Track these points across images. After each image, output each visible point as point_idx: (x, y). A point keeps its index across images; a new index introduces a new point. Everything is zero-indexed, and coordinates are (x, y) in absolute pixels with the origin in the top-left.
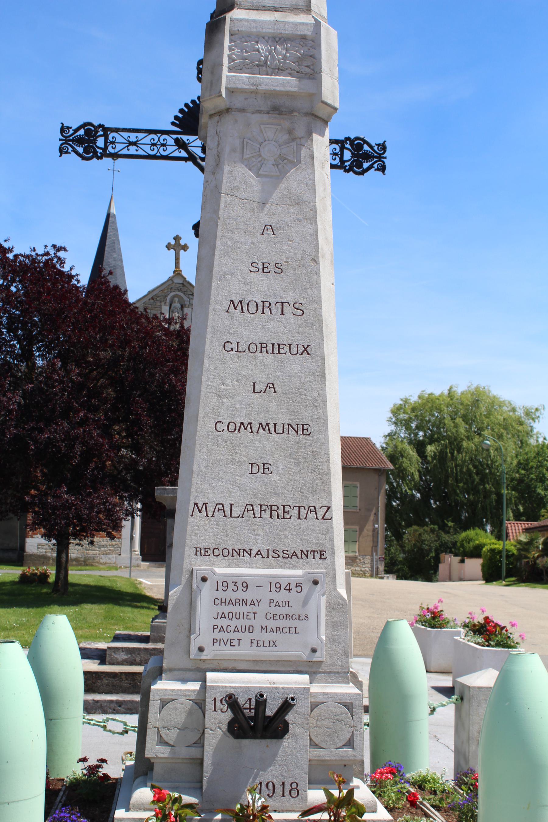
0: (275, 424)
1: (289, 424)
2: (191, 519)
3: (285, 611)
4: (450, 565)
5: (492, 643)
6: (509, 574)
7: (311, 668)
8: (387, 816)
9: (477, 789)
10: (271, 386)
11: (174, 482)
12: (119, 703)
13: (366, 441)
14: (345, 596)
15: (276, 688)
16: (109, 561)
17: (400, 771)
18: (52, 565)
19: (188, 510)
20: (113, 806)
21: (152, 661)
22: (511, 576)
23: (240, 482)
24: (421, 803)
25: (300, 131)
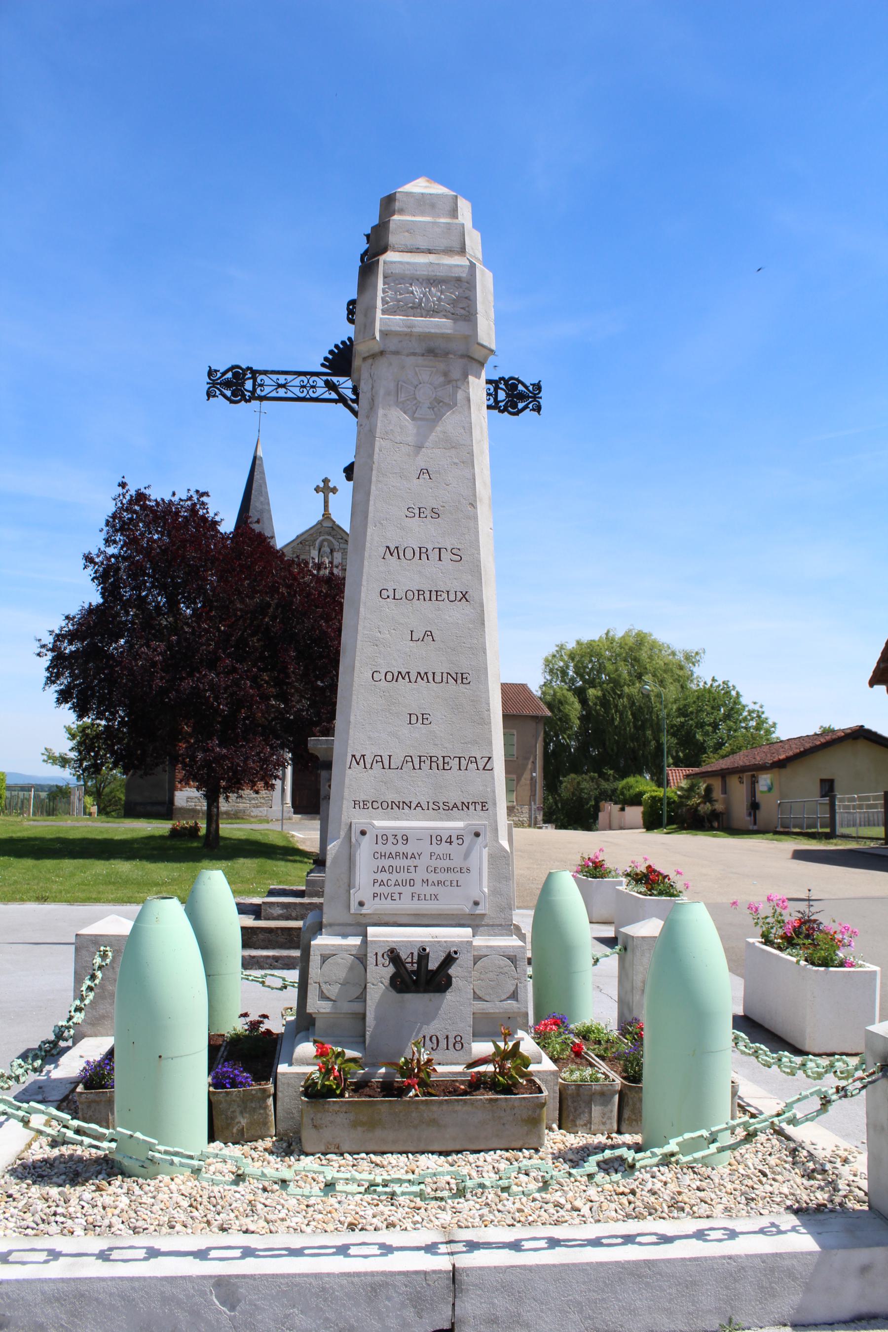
0: (434, 673)
2: (349, 772)
3: (446, 863)
4: (610, 813)
5: (655, 892)
6: (671, 821)
7: (473, 921)
8: (552, 1067)
9: (642, 1038)
11: (329, 731)
12: (276, 959)
13: (523, 688)
15: (439, 942)
16: (259, 814)
17: (564, 1022)
18: (202, 819)
20: (276, 1061)
21: (311, 917)
22: (673, 824)
24: (586, 1053)
25: (456, 374)
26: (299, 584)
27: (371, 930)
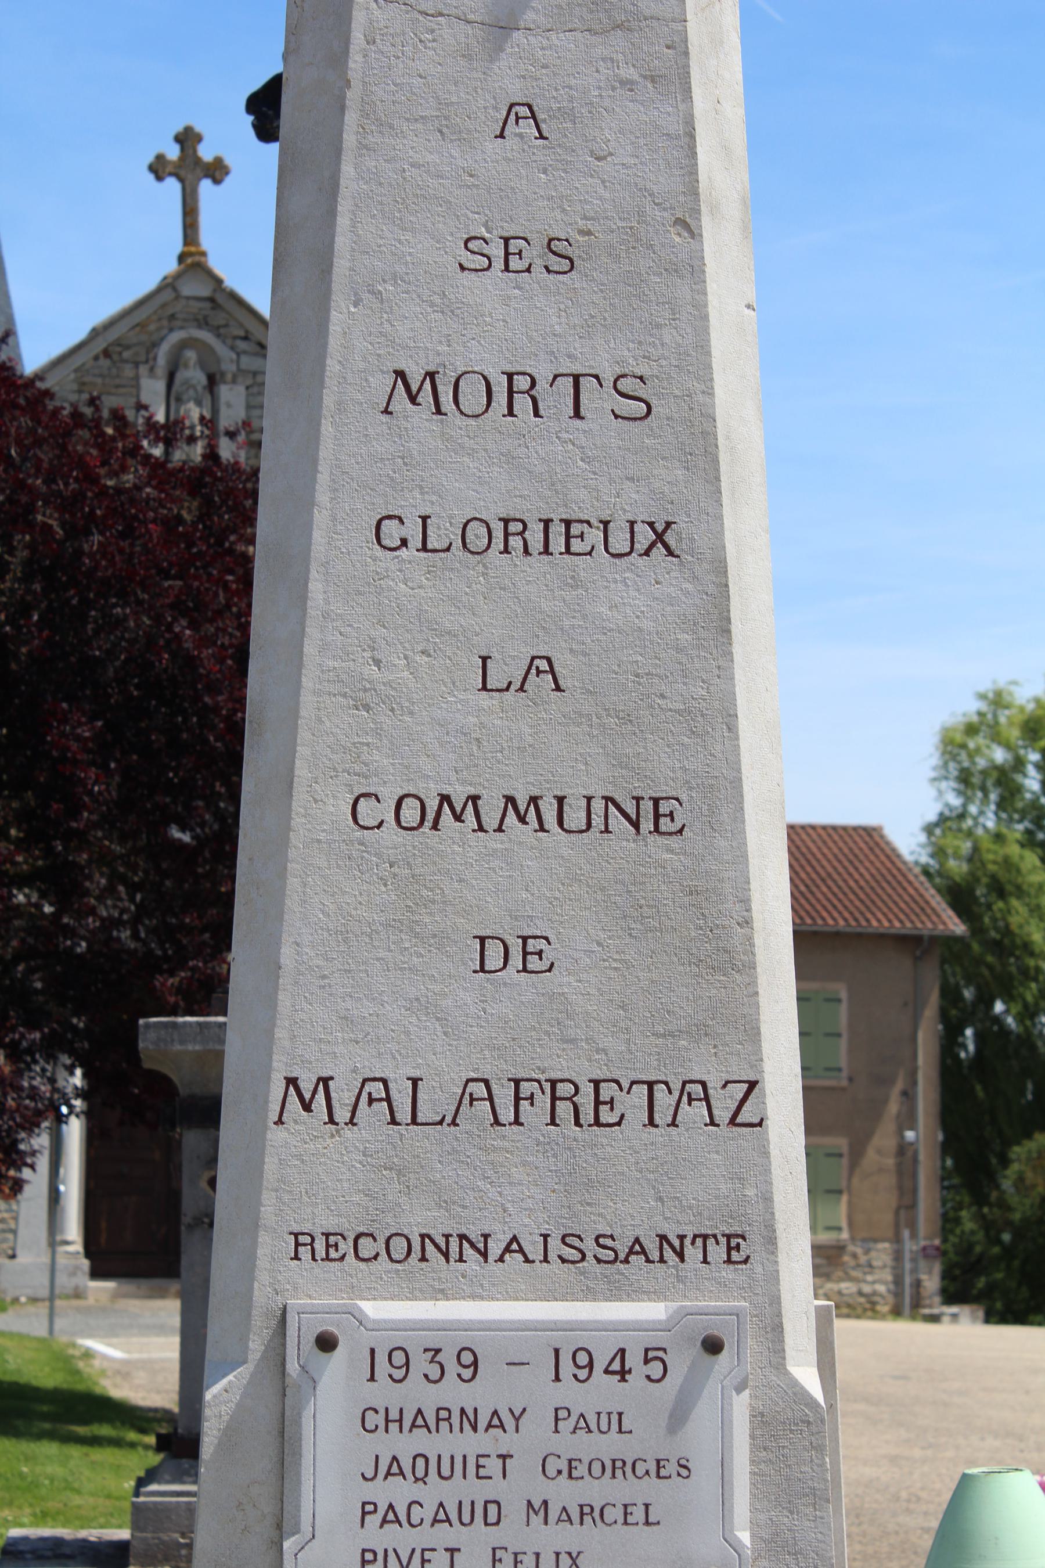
0: (560, 800)
1: (608, 799)
2: (276, 1135)
3: (608, 1446)
10: (540, 666)
11: (209, 993)
13: (869, 838)
14: (817, 1392)
19: (266, 1102)
23: (444, 1003)
26: (104, 491)
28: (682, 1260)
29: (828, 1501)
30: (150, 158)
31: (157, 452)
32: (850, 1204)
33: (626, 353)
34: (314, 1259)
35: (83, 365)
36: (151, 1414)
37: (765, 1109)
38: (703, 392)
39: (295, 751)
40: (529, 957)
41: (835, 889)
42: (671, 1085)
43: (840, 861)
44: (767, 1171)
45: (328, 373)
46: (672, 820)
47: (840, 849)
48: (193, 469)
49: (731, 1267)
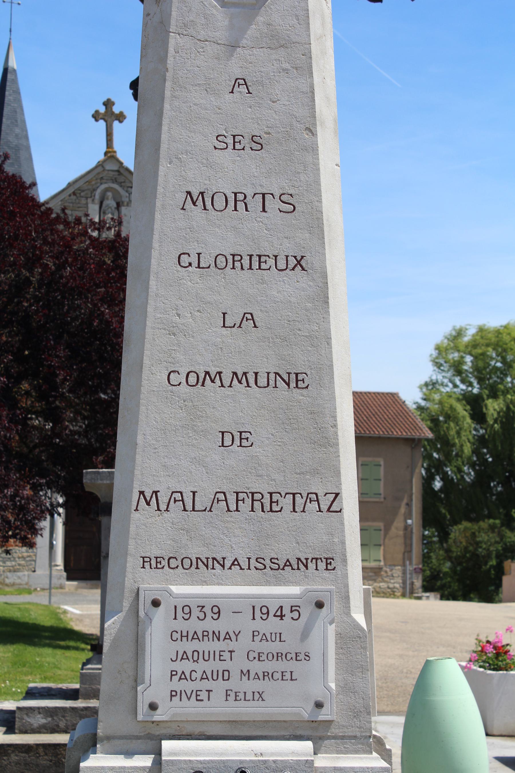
0: (256, 374)
1: (276, 373)
2: (135, 515)
3: (276, 647)
10: (249, 317)
11: (110, 462)
13: (392, 399)
15: (265, 762)
16: (18, 581)
19: (131, 501)
21: (82, 727)
27: (166, 745)
28: (307, 569)
29: (368, 670)
30: (93, 112)
31: (95, 234)
32: (384, 550)
33: (285, 184)
34: (151, 568)
35: (64, 198)
36: (91, 637)
37: (342, 505)
38: (317, 201)
39: (144, 353)
40: (242, 440)
41: (379, 419)
42: (303, 495)
43: (380, 407)
44: (343, 531)
45: (158, 192)
46: (304, 382)
47: (381, 402)
48: (110, 241)
49: (328, 571)
